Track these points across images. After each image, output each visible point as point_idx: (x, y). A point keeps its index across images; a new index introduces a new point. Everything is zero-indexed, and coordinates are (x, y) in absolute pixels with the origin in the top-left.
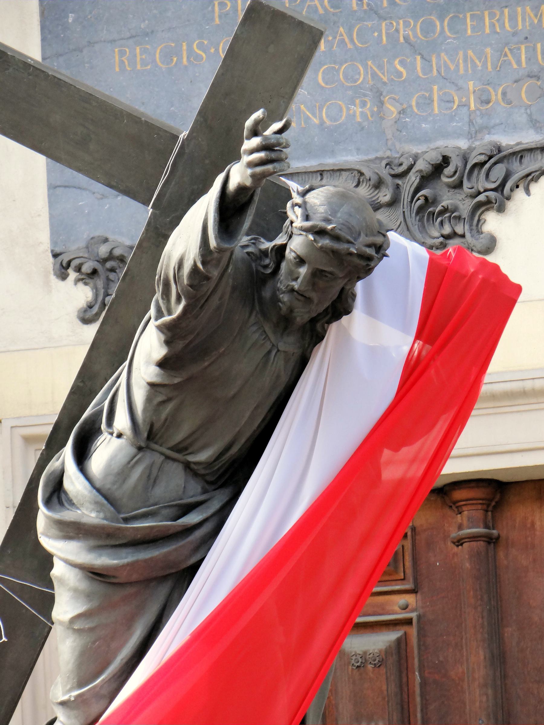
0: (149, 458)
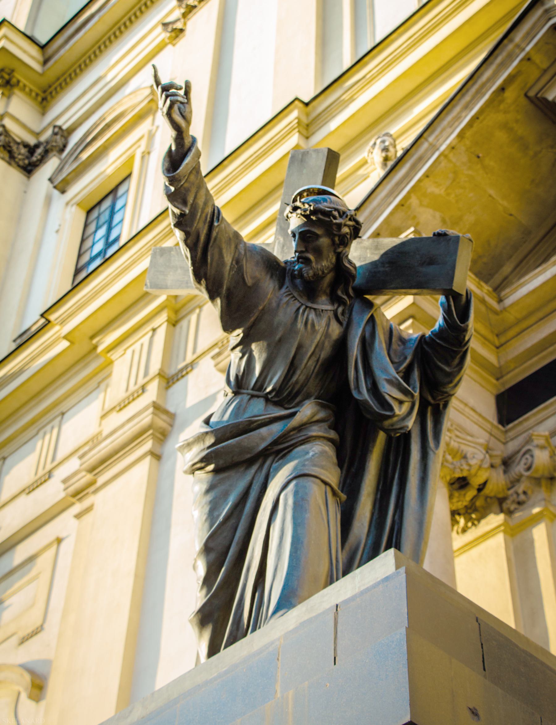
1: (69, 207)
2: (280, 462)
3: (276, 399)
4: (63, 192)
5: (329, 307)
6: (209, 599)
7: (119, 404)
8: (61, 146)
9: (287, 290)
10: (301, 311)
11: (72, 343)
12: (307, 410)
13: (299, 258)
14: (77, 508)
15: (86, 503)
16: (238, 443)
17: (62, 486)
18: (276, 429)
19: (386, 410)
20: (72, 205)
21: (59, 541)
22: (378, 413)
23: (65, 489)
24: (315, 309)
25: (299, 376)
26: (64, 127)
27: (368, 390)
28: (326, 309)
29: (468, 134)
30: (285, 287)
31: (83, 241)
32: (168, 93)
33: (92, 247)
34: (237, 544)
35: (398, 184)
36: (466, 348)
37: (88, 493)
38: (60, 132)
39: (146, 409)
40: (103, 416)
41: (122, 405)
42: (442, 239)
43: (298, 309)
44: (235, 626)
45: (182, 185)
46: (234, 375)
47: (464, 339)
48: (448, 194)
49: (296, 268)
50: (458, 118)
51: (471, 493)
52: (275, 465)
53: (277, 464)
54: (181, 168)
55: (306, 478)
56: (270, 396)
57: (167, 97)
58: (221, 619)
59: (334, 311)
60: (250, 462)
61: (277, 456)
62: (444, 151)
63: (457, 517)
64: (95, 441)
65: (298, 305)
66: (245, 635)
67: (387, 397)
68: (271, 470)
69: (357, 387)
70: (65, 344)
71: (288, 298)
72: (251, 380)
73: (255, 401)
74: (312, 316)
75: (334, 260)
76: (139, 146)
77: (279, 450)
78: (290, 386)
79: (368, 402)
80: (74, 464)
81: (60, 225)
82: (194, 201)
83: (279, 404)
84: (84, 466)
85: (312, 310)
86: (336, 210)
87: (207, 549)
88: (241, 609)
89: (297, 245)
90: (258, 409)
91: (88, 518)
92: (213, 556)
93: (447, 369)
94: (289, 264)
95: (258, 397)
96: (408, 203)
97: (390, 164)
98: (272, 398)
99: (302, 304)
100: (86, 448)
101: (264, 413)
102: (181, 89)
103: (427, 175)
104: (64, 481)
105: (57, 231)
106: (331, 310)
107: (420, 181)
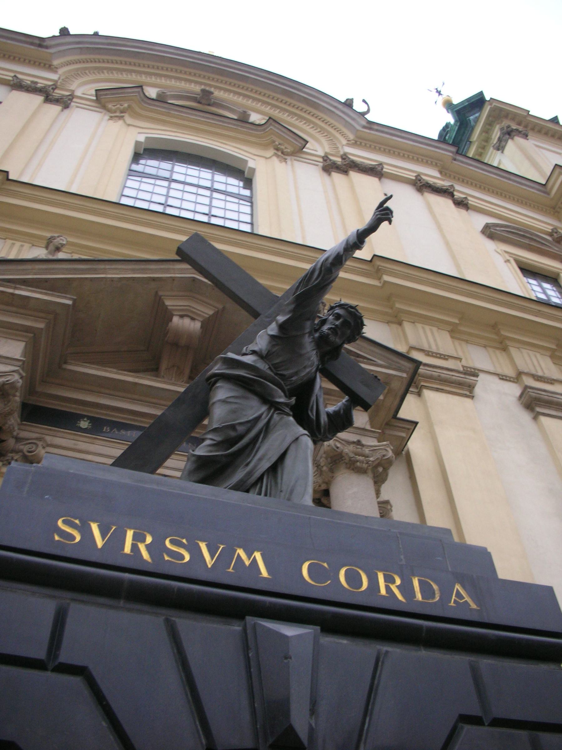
50: (126, 271)
103: (91, 279)
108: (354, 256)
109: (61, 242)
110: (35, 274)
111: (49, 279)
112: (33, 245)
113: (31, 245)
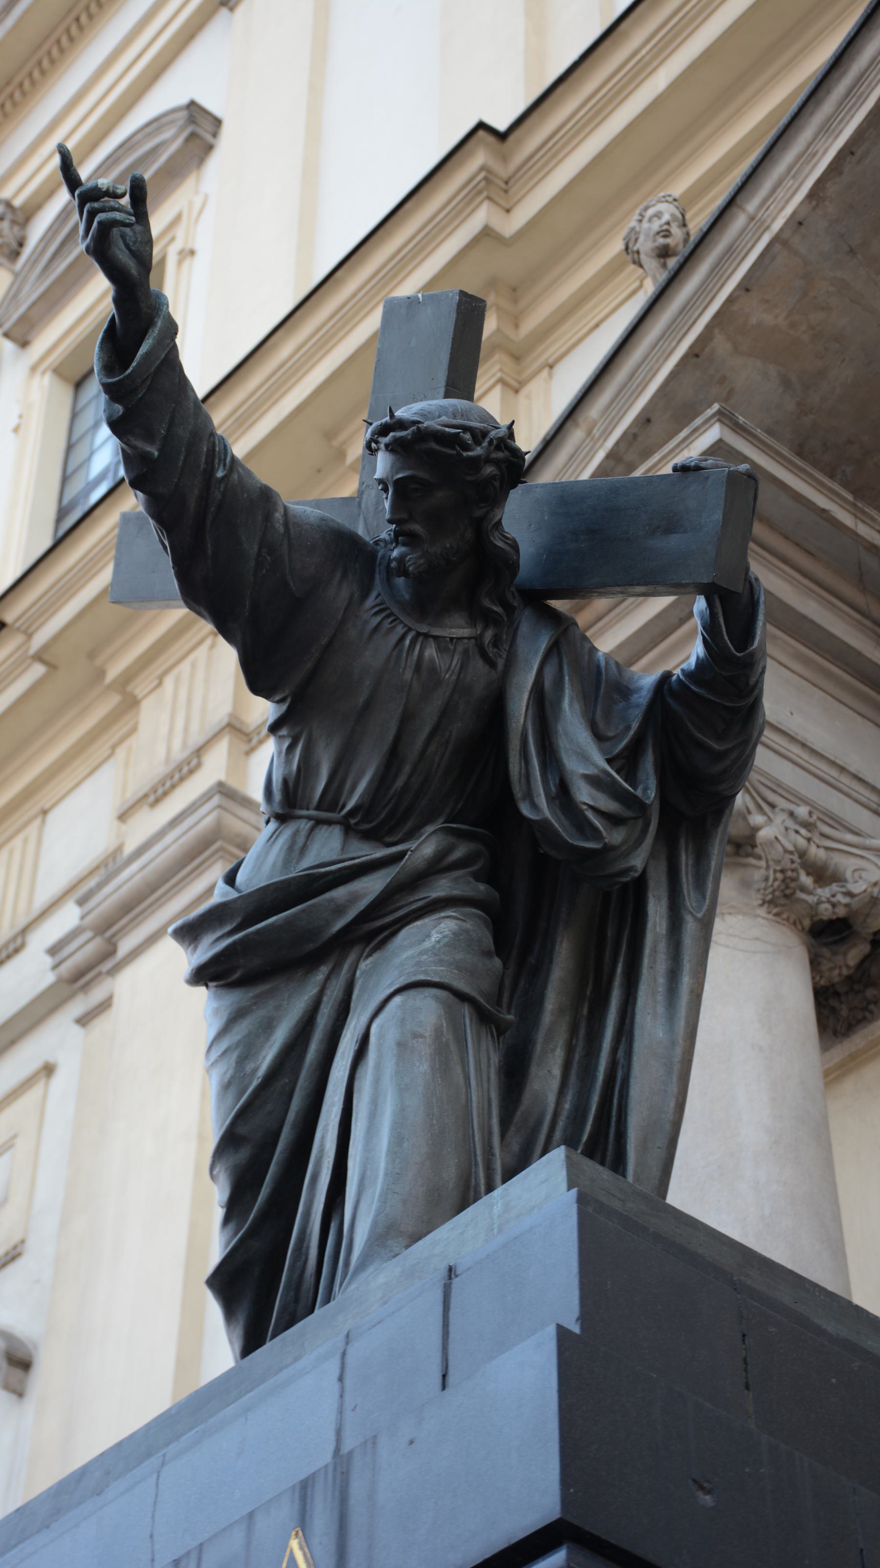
0: (288, 832)
1: (37, 377)
2: (376, 956)
3: (366, 826)
4: (24, 344)
5: (466, 632)
6: (241, 1241)
7: (154, 790)
8: (14, 245)
9: (378, 601)
10: (407, 642)
11: (52, 666)
12: (425, 847)
13: (397, 534)
14: (78, 1006)
15: (97, 995)
16: (288, 922)
17: (49, 961)
18: (372, 886)
19: (587, 839)
20: (44, 373)
21: (48, 1070)
22: (572, 845)
23: (55, 967)
24: (436, 638)
25: (410, 776)
26: (17, 202)
27: (550, 799)
28: (459, 636)
29: (832, 189)
30: (374, 594)
31: (70, 448)
32: (96, 205)
33: (88, 459)
34: (294, 1126)
35: (684, 310)
36: (752, 699)
37: (99, 974)
38: (9, 216)
39: (206, 797)
40: (123, 817)
41: (160, 791)
42: (691, 476)
43: (402, 638)
44: (292, 1294)
45: (141, 398)
46: (280, 780)
47: (747, 683)
48: (793, 325)
49: (395, 554)
50: (808, 156)
51: (854, 955)
52: (364, 965)
53: (369, 961)
54: (134, 364)
55: (421, 990)
56: (352, 821)
57: (92, 214)
58: (265, 1280)
59: (475, 638)
60: (310, 961)
61: (369, 943)
62: (782, 230)
63: (833, 1002)
64: (110, 864)
65: (400, 630)
66: (312, 1311)
67: (590, 815)
68: (358, 973)
69: (529, 795)
70: (38, 670)
71: (378, 619)
72: (313, 789)
73: (323, 832)
74: (431, 651)
75: (469, 535)
76: (173, 239)
77: (373, 930)
78: (390, 799)
79: (552, 825)
80: (69, 917)
81: (20, 417)
82: (169, 430)
83: (371, 836)
84: (89, 919)
85: (431, 640)
86: (465, 429)
87: (229, 1142)
88: (303, 1258)
89: (394, 507)
90: (328, 847)
91: (101, 1025)
92: (243, 1155)
93: (716, 746)
94: (382, 544)
95: (329, 823)
96: (708, 350)
97: (673, 263)
98: (357, 824)
99: (410, 629)
100: (92, 883)
101: (340, 857)
102: (122, 195)
103: (745, 287)
104: (53, 951)
105: (16, 430)
106: (469, 638)
107: (730, 300)
108: (201, 391)
109: (656, 225)
110: (606, 434)
111: (645, 409)
112: (551, 367)
113: (545, 373)
